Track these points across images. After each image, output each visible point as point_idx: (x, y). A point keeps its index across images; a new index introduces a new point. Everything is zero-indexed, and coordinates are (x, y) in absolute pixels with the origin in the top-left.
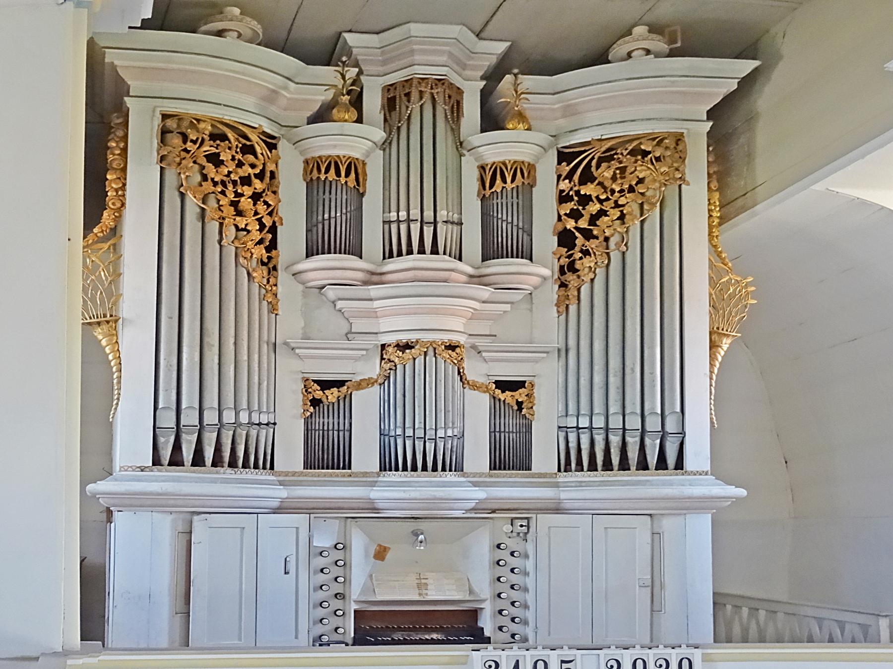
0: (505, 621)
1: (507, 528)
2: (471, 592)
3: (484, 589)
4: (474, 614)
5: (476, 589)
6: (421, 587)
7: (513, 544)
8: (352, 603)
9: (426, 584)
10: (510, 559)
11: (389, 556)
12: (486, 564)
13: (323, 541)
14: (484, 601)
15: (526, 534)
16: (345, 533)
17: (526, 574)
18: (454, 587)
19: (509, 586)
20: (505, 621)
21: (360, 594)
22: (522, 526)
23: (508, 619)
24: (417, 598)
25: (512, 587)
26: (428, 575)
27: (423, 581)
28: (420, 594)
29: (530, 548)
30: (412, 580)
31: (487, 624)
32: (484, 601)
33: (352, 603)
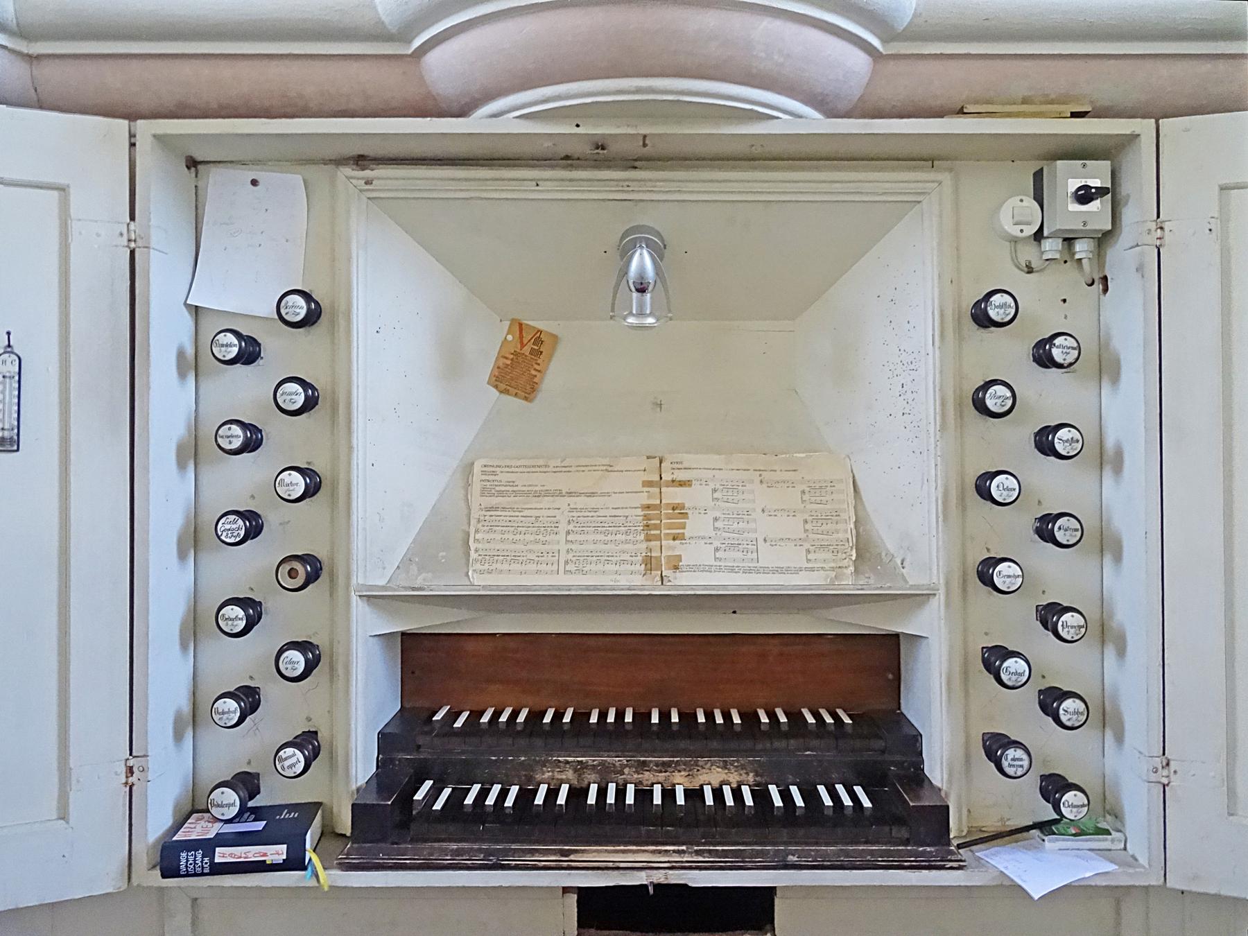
0: (1019, 716)
1: (1018, 213)
2: (865, 551)
3: (919, 538)
4: (884, 656)
5: (888, 540)
6: (662, 521)
7: (1044, 302)
8: (359, 608)
9: (679, 510)
10: (1041, 644)
11: (556, 376)
12: (927, 406)
13: (245, 287)
14: (918, 599)
15: (1103, 239)
16: (330, 248)
17: (1107, 460)
18: (793, 527)
19: (1026, 522)
20: (1019, 716)
21: (407, 560)
22: (1085, 195)
23: (1023, 612)
24: (631, 580)
25: (1045, 529)
26: (688, 459)
27: (673, 495)
28: (650, 563)
29: (1125, 317)
30: (625, 494)
31: (939, 714)
32: (918, 599)
33: (359, 608)
